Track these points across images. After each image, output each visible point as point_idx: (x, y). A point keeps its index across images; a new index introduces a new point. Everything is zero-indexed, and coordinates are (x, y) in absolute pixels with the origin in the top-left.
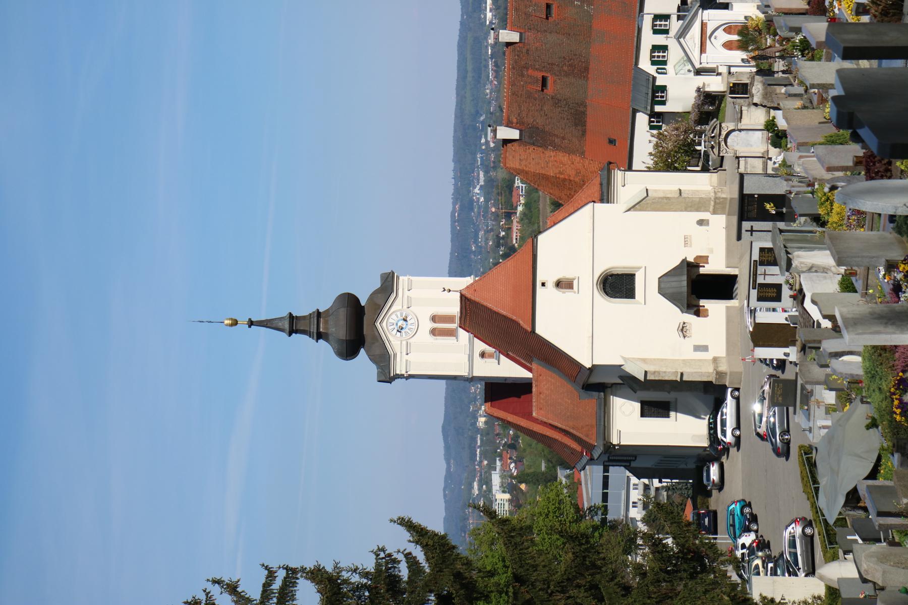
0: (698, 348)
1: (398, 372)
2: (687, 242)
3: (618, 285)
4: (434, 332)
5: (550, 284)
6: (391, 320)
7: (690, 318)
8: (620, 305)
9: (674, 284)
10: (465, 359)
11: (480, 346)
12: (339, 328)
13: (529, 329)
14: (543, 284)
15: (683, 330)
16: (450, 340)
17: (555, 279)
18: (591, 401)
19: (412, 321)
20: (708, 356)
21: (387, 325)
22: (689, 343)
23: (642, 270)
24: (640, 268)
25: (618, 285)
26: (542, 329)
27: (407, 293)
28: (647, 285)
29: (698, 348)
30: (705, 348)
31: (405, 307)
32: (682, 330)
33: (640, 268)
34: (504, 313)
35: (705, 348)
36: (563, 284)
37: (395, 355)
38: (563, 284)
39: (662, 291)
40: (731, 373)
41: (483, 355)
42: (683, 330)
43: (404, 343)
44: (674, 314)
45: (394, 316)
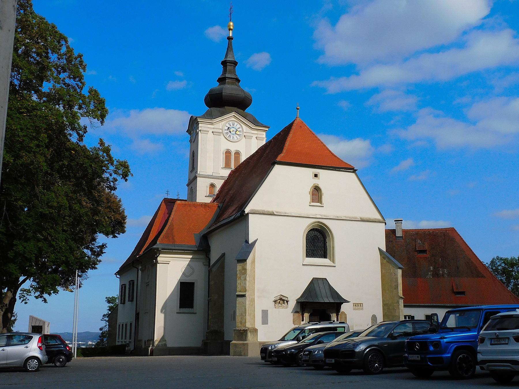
0: (265, 313)
1: (200, 125)
2: (358, 306)
3: (318, 242)
4: (228, 153)
5: (316, 181)
6: (236, 124)
7: (292, 303)
8: (300, 244)
9: (323, 292)
10: (210, 173)
11: (219, 184)
12: (229, 89)
13: (279, 159)
14: (316, 176)
15: (282, 301)
16: (222, 163)
17: (321, 186)
18: (193, 242)
19: (236, 138)
20: (258, 324)
21: (230, 120)
22: (269, 305)
23: (331, 264)
24: (334, 262)
25: (318, 242)
26: (278, 170)
27: (255, 136)
28: (318, 268)
29: (265, 313)
30: (265, 321)
31: (245, 134)
32: (281, 299)
33: (334, 262)
34: (287, 144)
35: (265, 321)
36: (317, 193)
37: (212, 124)
38: (317, 193)
39: (315, 281)
40: (247, 344)
41: (212, 186)
42: (282, 301)
43: (221, 131)
44: (295, 292)
45: (239, 126)
